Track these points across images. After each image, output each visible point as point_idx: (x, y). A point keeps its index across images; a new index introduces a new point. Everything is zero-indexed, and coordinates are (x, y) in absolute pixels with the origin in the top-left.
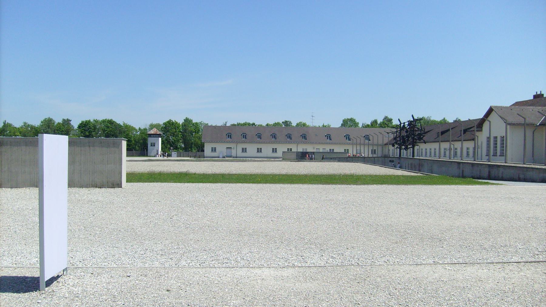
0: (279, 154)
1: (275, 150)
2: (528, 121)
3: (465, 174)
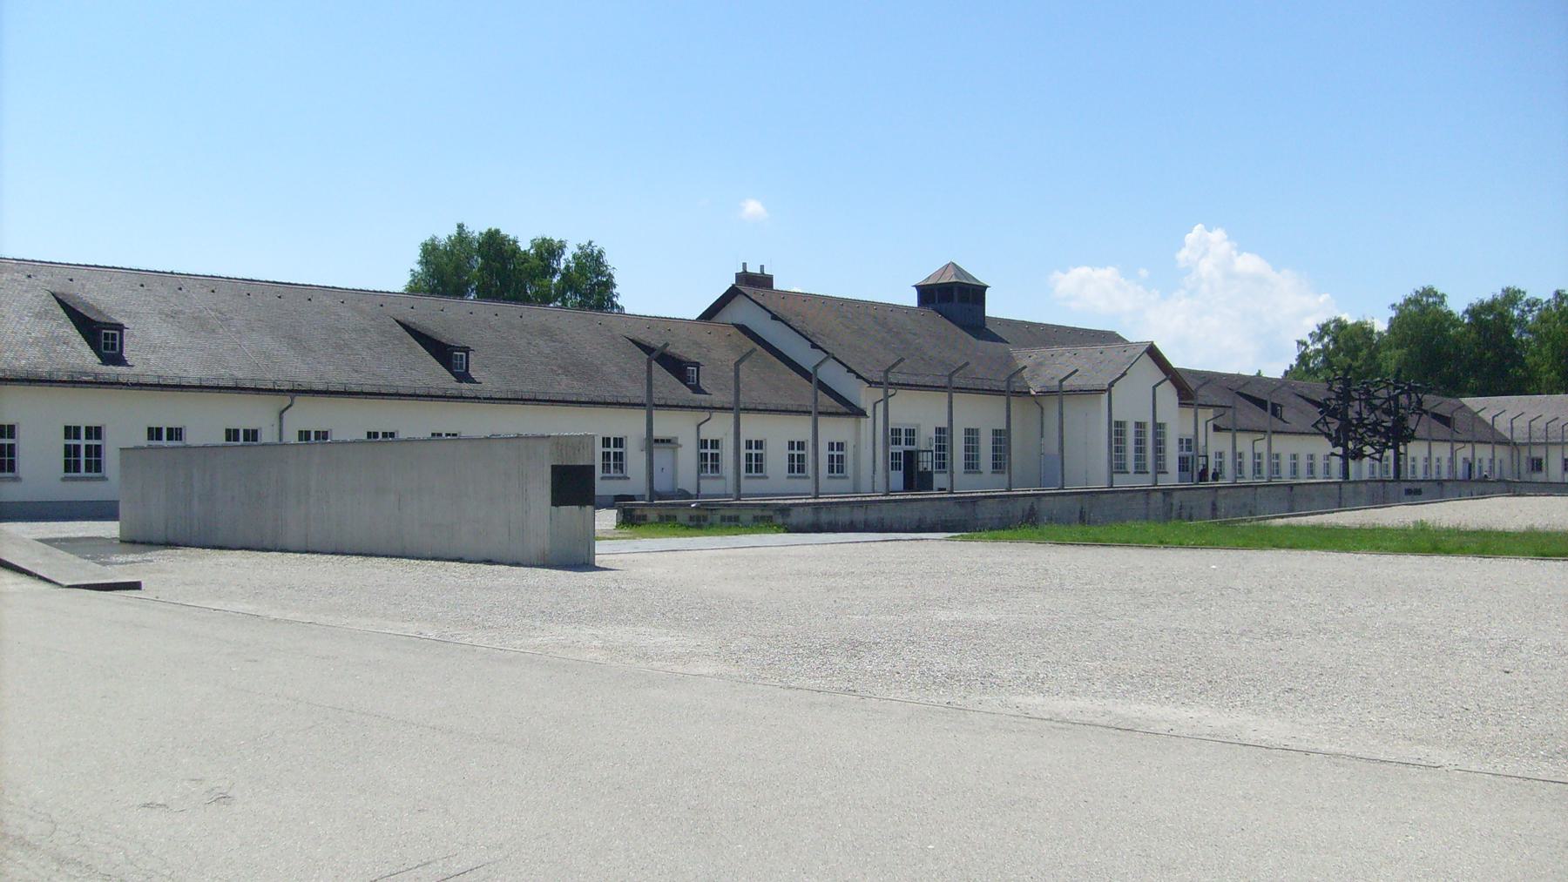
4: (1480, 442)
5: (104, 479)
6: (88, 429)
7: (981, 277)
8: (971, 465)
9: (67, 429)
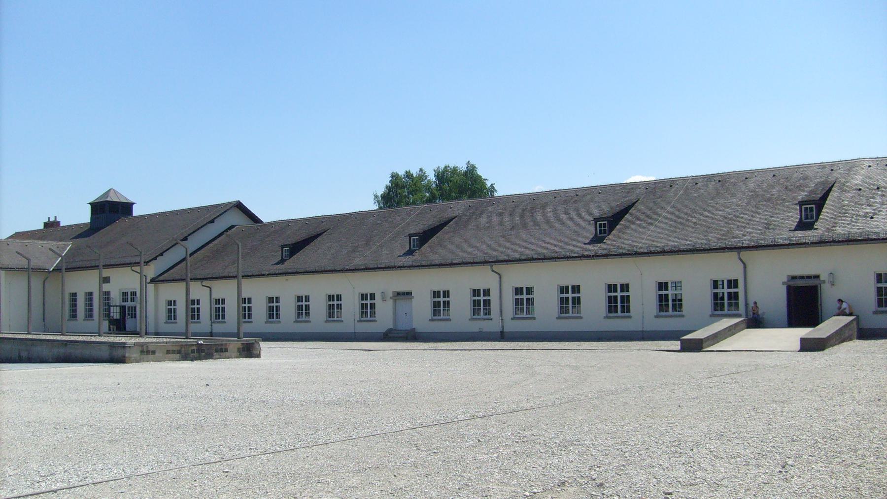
2: (34, 263)
5: (280, 322)
6: (573, 287)
7: (131, 199)
8: (89, 315)
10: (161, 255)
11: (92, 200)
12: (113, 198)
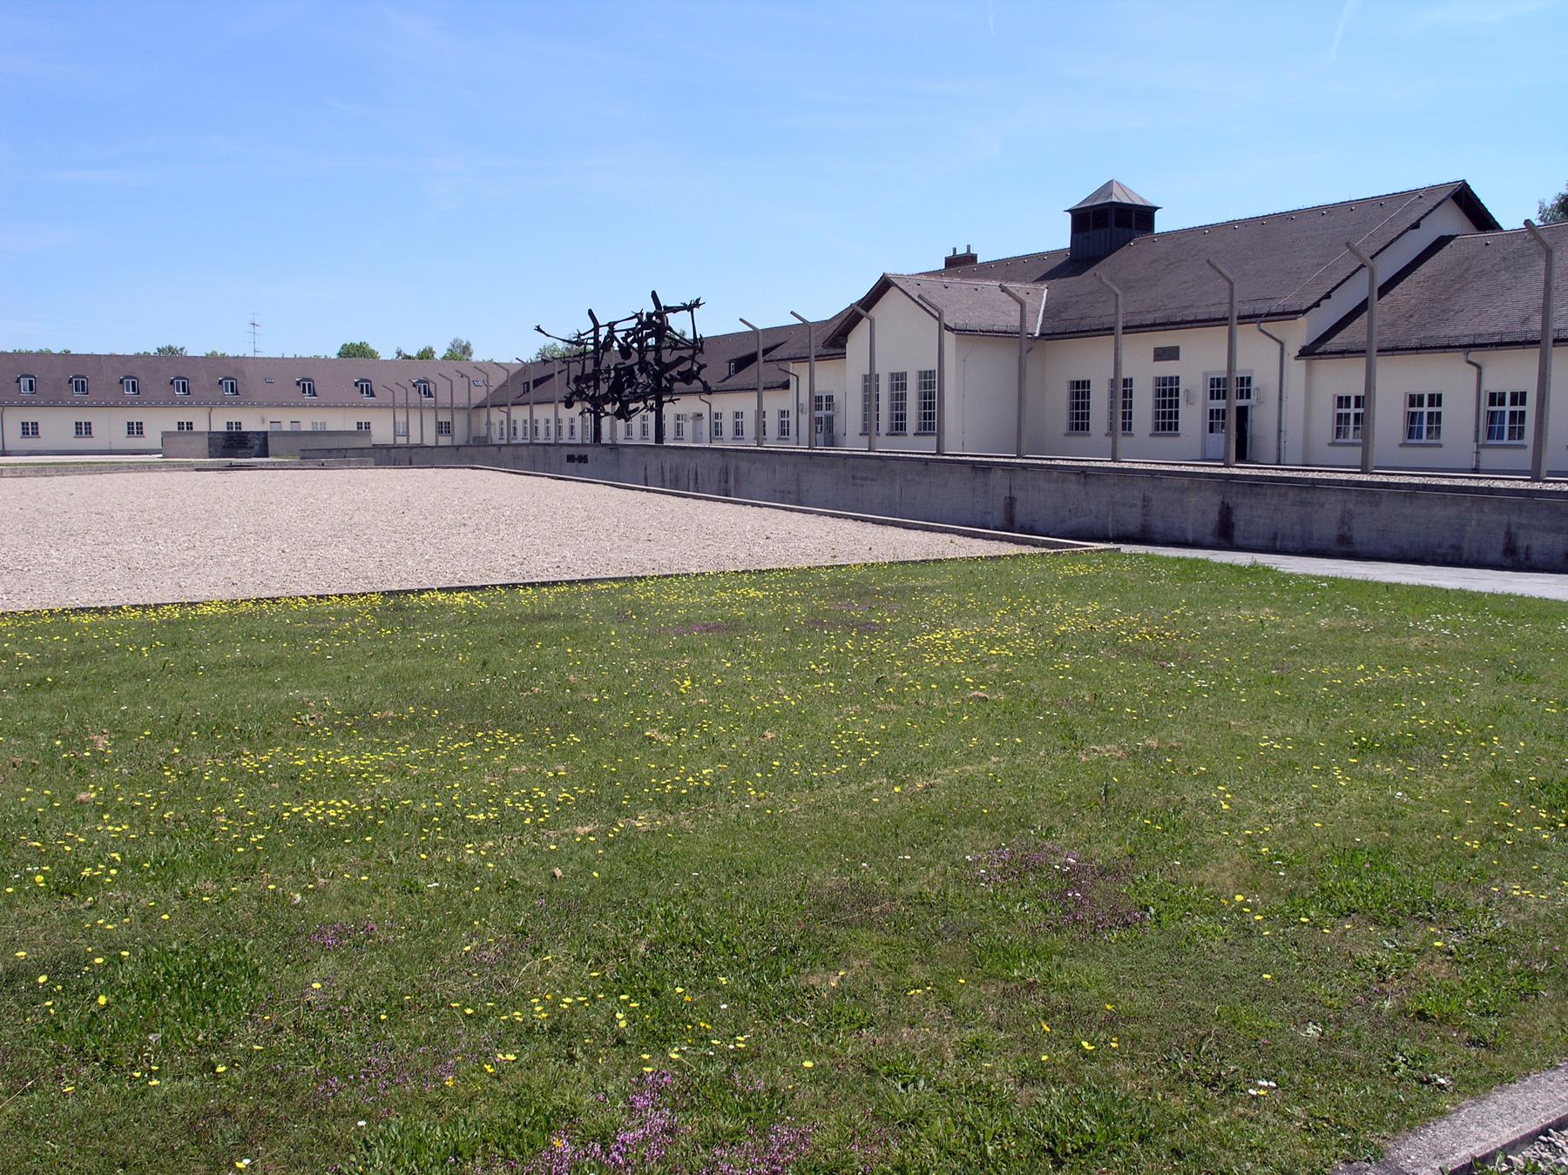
0: (152, 438)
1: (135, 429)
3: (1021, 515)
4: (1245, 319)
6: (1431, 397)
7: (1151, 200)
8: (898, 427)
9: (1412, 398)
10: (1327, 296)
11: (1073, 204)
12: (1118, 197)
